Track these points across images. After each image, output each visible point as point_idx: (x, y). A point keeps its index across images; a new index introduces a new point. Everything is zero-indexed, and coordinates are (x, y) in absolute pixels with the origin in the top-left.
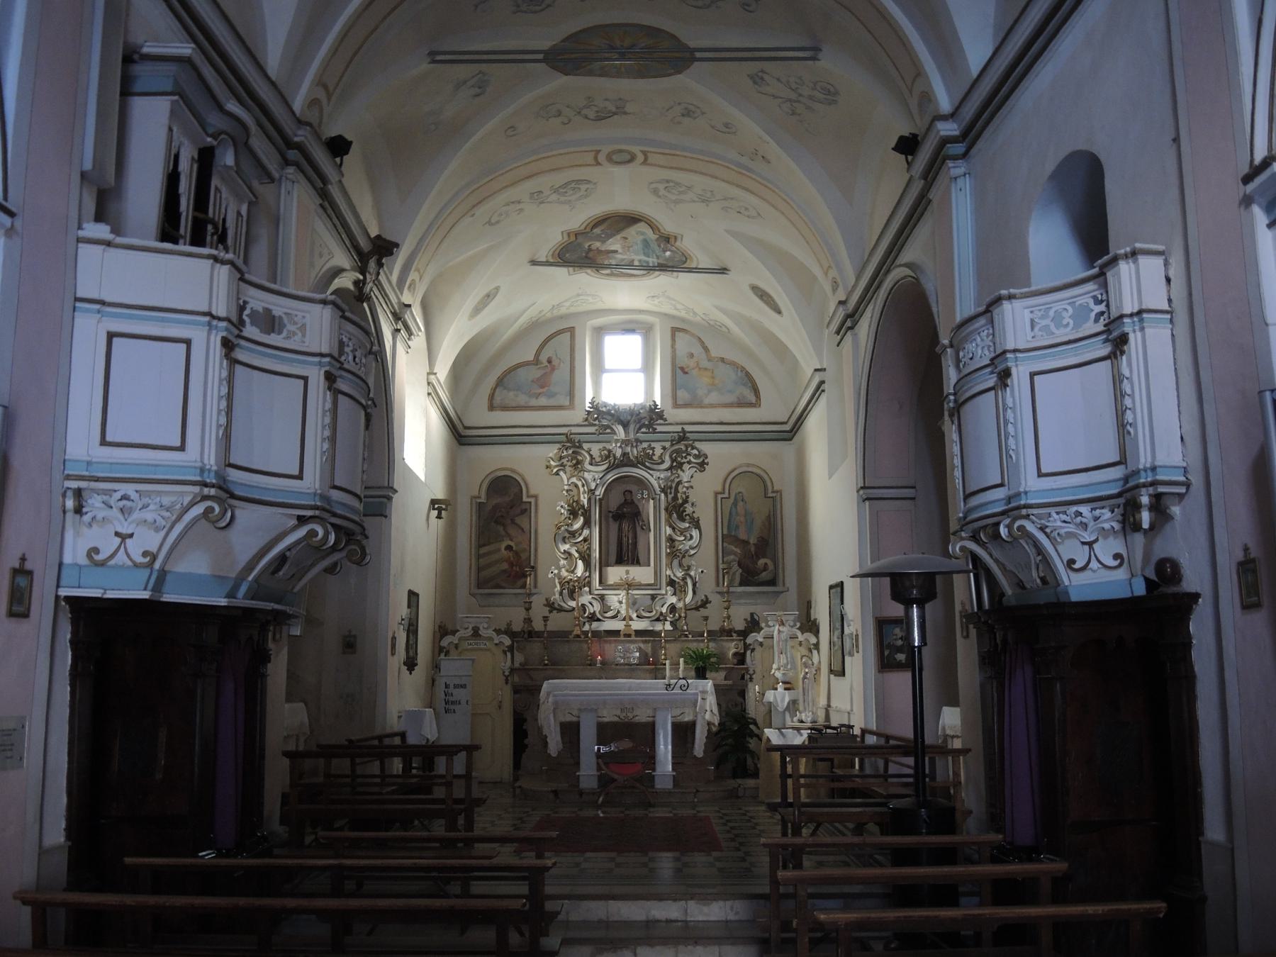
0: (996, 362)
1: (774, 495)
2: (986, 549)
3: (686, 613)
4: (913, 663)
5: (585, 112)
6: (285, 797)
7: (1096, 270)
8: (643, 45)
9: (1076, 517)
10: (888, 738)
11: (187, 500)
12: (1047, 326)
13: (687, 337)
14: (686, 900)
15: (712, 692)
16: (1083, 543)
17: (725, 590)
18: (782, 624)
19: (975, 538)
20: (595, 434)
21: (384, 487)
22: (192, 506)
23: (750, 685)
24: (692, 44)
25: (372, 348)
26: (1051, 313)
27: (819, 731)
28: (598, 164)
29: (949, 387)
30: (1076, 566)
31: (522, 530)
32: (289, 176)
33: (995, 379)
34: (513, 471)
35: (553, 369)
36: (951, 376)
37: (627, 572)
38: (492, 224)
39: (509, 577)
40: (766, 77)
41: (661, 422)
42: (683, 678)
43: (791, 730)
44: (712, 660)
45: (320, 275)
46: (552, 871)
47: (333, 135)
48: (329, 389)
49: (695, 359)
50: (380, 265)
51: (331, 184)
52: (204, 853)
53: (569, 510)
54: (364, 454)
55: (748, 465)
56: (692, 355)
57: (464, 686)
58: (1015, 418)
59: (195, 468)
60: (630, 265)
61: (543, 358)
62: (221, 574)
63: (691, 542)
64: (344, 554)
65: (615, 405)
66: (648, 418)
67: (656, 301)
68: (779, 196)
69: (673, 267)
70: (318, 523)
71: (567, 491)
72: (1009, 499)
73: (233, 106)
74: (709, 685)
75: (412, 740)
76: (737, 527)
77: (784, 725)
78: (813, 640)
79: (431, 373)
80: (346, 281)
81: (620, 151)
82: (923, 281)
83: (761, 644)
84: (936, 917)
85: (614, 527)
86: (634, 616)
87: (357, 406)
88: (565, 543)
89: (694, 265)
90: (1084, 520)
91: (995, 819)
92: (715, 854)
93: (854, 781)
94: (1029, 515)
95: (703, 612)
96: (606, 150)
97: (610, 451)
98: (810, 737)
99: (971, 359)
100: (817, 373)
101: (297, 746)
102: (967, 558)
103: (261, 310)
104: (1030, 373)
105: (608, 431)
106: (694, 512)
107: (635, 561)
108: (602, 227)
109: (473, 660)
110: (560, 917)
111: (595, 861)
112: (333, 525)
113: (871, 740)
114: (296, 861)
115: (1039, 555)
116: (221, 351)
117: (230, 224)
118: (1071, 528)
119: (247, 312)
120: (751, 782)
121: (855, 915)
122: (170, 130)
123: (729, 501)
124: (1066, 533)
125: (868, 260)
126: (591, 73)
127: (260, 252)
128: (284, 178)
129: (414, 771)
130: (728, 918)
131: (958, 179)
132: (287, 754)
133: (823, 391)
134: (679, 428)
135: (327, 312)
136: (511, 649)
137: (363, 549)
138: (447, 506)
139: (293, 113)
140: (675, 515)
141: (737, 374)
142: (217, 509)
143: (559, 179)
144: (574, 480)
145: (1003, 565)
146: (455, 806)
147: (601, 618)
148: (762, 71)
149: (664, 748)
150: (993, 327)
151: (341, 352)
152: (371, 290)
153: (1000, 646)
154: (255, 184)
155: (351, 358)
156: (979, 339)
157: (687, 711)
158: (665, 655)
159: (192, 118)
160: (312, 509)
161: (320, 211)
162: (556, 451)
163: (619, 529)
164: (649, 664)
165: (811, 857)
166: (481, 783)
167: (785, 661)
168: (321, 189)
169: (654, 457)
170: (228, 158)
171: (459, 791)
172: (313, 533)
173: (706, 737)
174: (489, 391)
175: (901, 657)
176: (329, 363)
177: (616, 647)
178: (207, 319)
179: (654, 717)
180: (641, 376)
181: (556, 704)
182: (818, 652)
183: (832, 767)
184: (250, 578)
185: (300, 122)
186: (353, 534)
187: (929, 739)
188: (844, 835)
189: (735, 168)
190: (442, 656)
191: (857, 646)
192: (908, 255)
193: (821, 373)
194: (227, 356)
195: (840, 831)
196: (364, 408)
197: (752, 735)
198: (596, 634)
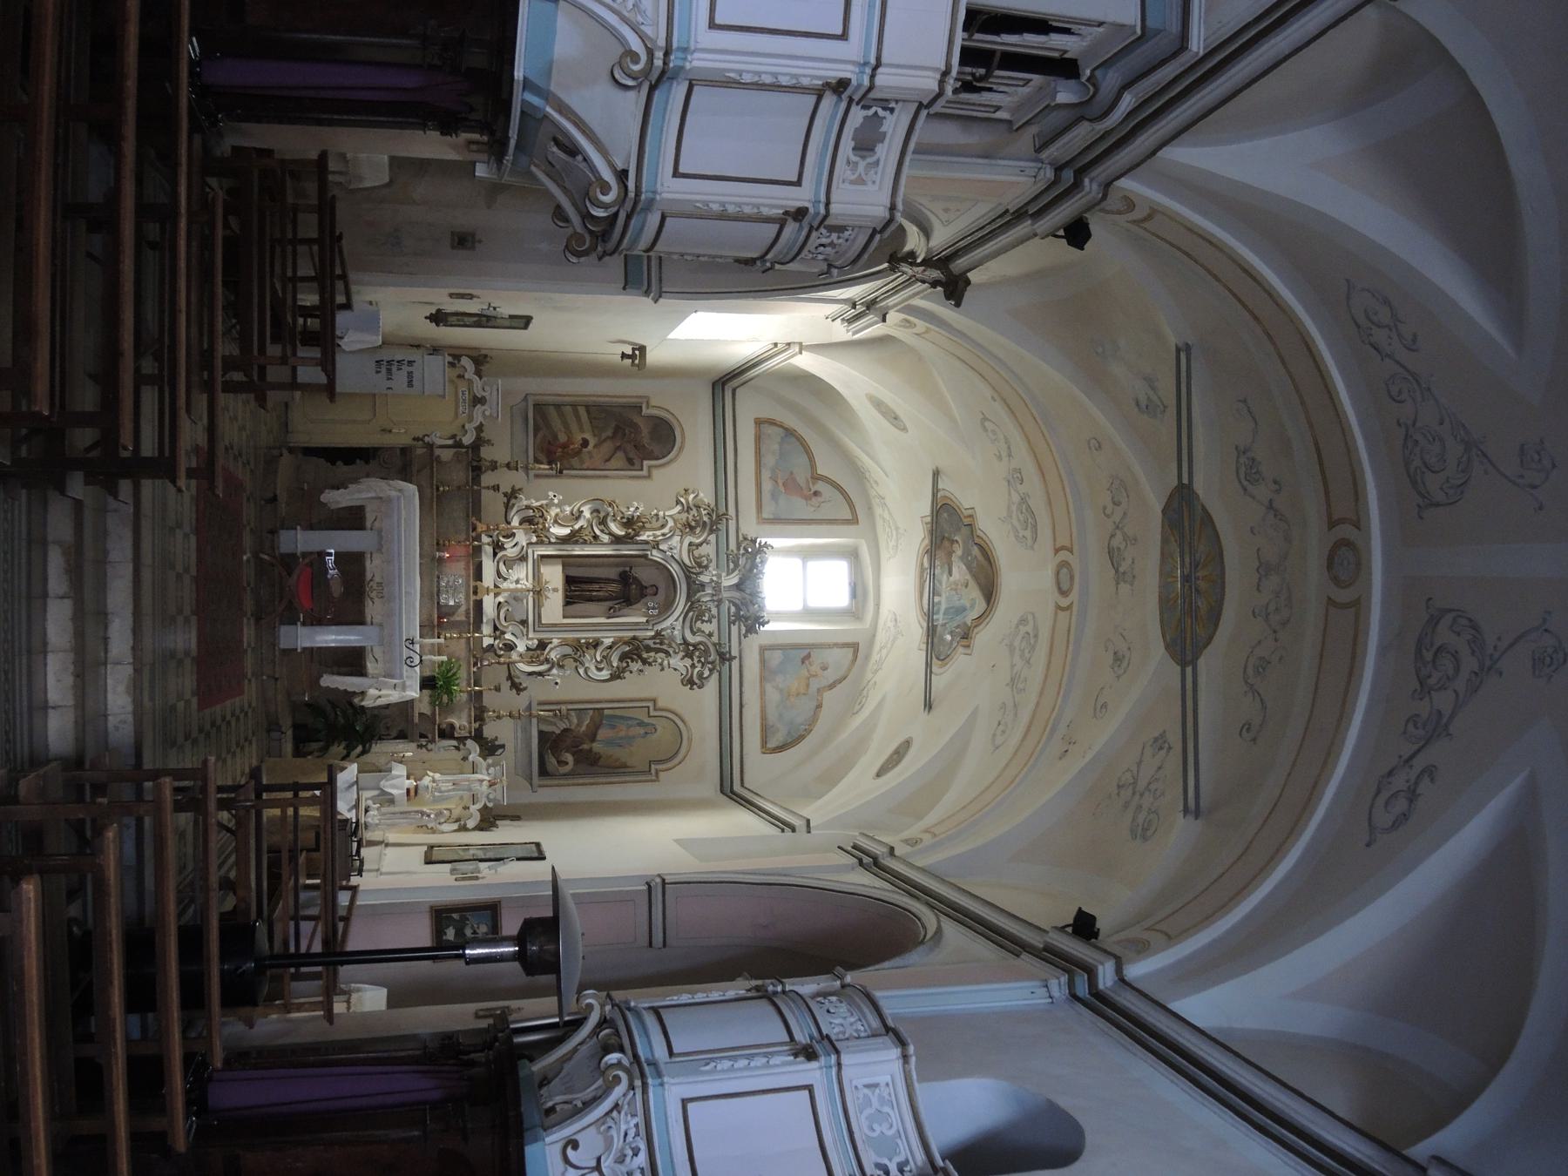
0: (826, 1042)
1: (653, 771)
2: (590, 1036)
3: (504, 663)
4: (440, 949)
5: (1119, 536)
6: (268, 153)
7: (940, 1163)
8: (1199, 604)
9: (633, 1149)
10: (346, 920)
11: (648, 30)
12: (869, 1103)
14: (134, 663)
15: (403, 697)
16: (599, 1160)
17: (534, 712)
18: (491, 784)
19: (604, 1022)
20: (727, 549)
21: (661, 288)
22: (640, 37)
23: (414, 745)
24: (1201, 662)
25: (836, 267)
26: (886, 1109)
27: (355, 833)
28: (1057, 551)
29: (792, 985)
30: (570, 1151)
32: (1042, 172)
33: (804, 1042)
34: (681, 448)
35: (807, 498)
36: (807, 987)
37: (555, 590)
38: (982, 424)
39: (549, 442)
40: (1163, 753)
41: (743, 631)
42: (421, 661)
43: (355, 796)
44: (445, 698)
45: (923, 210)
46: (171, 489)
47: (1091, 227)
48: (786, 213)
49: (820, 672)
50: (934, 284)
51: (1032, 225)
52: (196, 44)
53: (633, 517)
54: (704, 256)
55: (690, 740)
56: (825, 668)
57: (410, 384)
58: (757, 1068)
59: (688, 42)
60: (935, 592)
61: (820, 486)
62: (554, 71)
63: (593, 668)
64: (579, 229)
65: (763, 574)
66: (748, 617)
67: (890, 624)
68: (1020, 772)
69: (932, 642)
70: (619, 188)
71: (657, 515)
72: (653, 1064)
73: (1128, 101)
74: (413, 692)
75: (342, 318)
76: (613, 727)
77: (362, 789)
78: (471, 824)
79: (802, 348)
80: (914, 241)
81: (1072, 578)
82: (921, 949)
83: (465, 759)
84: (111, 983)
85: (613, 573)
86: (500, 599)
87: (764, 250)
88: (592, 513)
89: (934, 669)
90: (628, 1159)
91: (241, 1058)
92: (195, 701)
93: (290, 876)
94: (633, 1089)
95: (506, 685)
96: (1073, 560)
97: (706, 567)
98: (347, 821)
99: (828, 1011)
100: (804, 822)
101: (334, 173)
102: (576, 1013)
103: (883, 129)
104: (812, 1085)
105: (732, 566)
106: (631, 672)
107: (569, 601)
108: (980, 558)
109: (444, 397)
110: (110, 499)
111: (185, 548)
112: (616, 215)
113: (343, 898)
114: (184, 160)
115: (584, 1104)
116: (834, 78)
117: (985, 97)
118: (618, 1143)
119: (881, 113)
120: (288, 747)
121: (112, 878)
122: (1100, 24)
123: (646, 717)
124: (612, 1137)
125: (943, 881)
126: (1165, 541)
127: (951, 134)
128: (1040, 165)
129: (301, 321)
130: (110, 718)
131: (1045, 989)
132: (323, 156)
133: (783, 831)
134: (735, 653)
135: (882, 212)
136: (458, 445)
137: (585, 253)
138: (638, 365)
139: (1118, 178)
142: (607, 199)
143: (1038, 503)
144: (671, 523)
145: (570, 1059)
146: (256, 367)
147: (497, 558)
148: (1170, 748)
149: (331, 638)
150: (868, 1037)
151: (832, 229)
152: (904, 273)
153: (466, 1057)
154: (1033, 129)
155: (824, 241)
156: (852, 1020)
157: (380, 665)
158: (451, 638)
159: (1112, 53)
160: (636, 187)
161: (1001, 210)
162: (706, 501)
163: (609, 580)
164: (440, 617)
165: (192, 824)
166: (286, 405)
167: (443, 789)
168: (1026, 212)
170: (1066, 94)
171: (275, 374)
172: (605, 188)
173: (345, 690)
175: (450, 934)
176: (818, 213)
177: (461, 576)
178: (873, 61)
179: (372, 624)
180: (798, 607)
181: (389, 500)
182: (455, 831)
183: (309, 850)
184: (549, 109)
185: (1107, 185)
186: (604, 241)
187: (345, 971)
188: (220, 867)
189: (1053, 717)
190: (450, 359)
191: (463, 879)
192: (951, 929)
193: (805, 829)
194: (827, 85)
195: (223, 863)
196: (762, 257)
197: (349, 749)
198: (478, 551)
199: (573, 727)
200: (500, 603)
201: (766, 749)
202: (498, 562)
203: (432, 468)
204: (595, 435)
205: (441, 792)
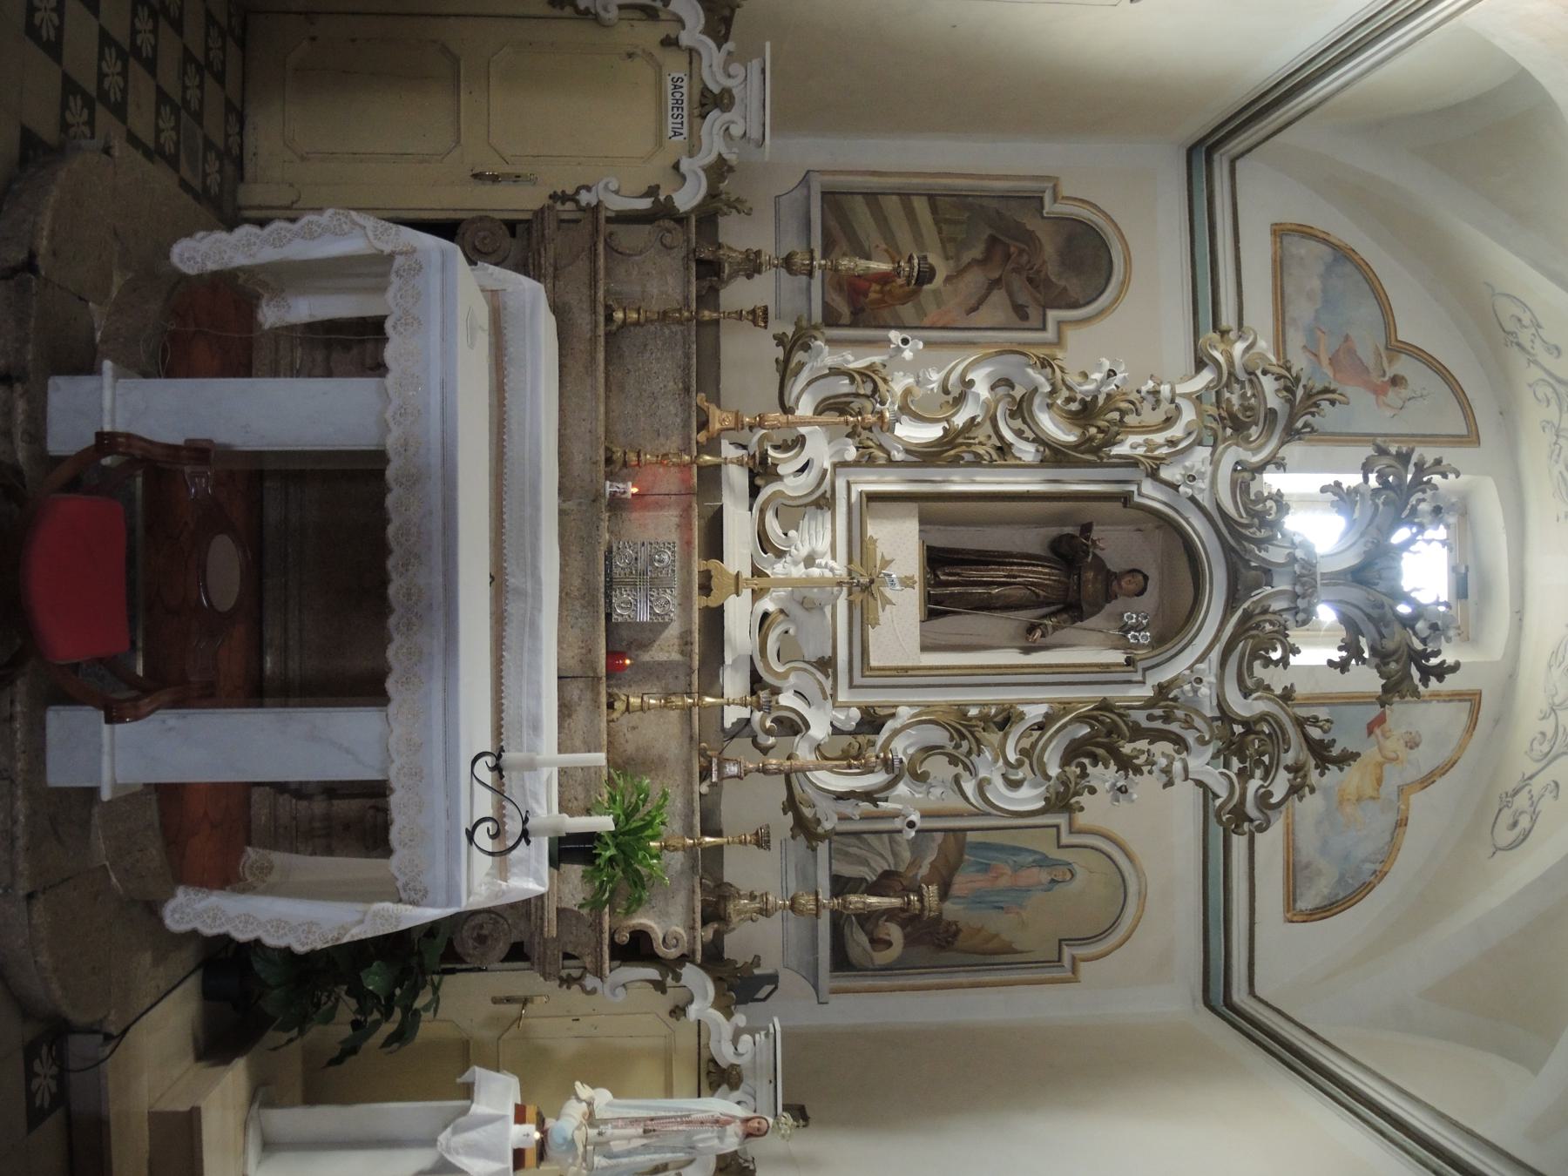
3: (779, 772)
13: (1457, 731)
31: (974, 309)
34: (1124, 284)
35: (1379, 391)
55: (1142, 896)
56: (1413, 744)
61: (1404, 366)
63: (998, 782)
71: (1155, 393)
76: (986, 868)
83: (678, 1011)
85: (1032, 540)
86: (768, 604)
88: (993, 388)
107: (935, 608)
140: (1086, 730)
141: (1363, 861)
144: (1188, 414)
164: (611, 654)
167: (617, 1146)
169: (1257, 664)
174: (1319, 224)
198: (711, 478)
199: (902, 869)
200: (766, 615)
201: (1294, 913)
202: (762, 512)
203: (593, 258)
204: (947, 258)
205: (610, 1155)
